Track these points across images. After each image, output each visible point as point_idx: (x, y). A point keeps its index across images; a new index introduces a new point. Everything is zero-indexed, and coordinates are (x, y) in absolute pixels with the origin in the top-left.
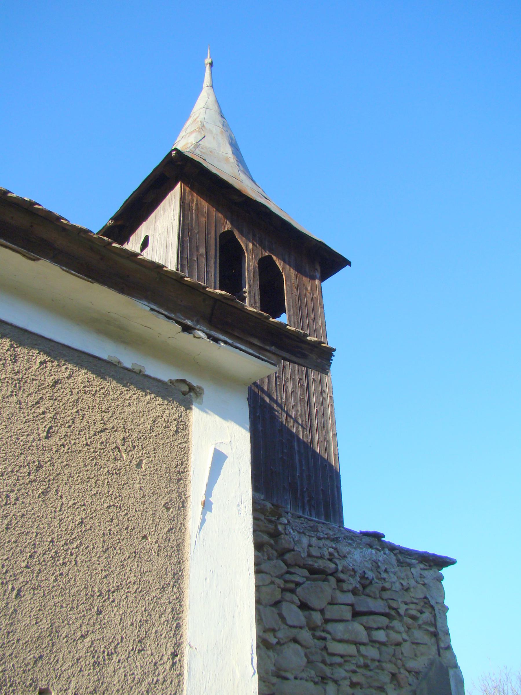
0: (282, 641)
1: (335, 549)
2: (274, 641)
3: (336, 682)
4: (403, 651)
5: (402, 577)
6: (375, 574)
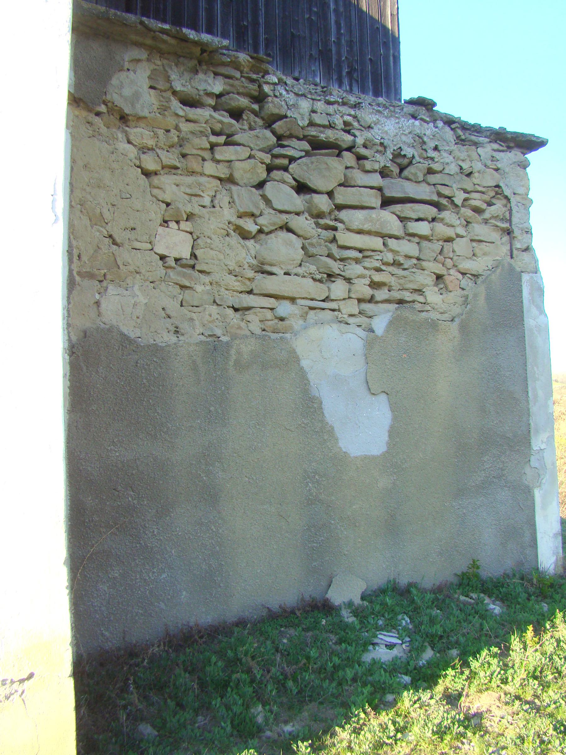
0: (266, 230)
1: (355, 117)
2: (253, 228)
3: (348, 280)
4: (456, 249)
5: (462, 158)
6: (417, 151)
